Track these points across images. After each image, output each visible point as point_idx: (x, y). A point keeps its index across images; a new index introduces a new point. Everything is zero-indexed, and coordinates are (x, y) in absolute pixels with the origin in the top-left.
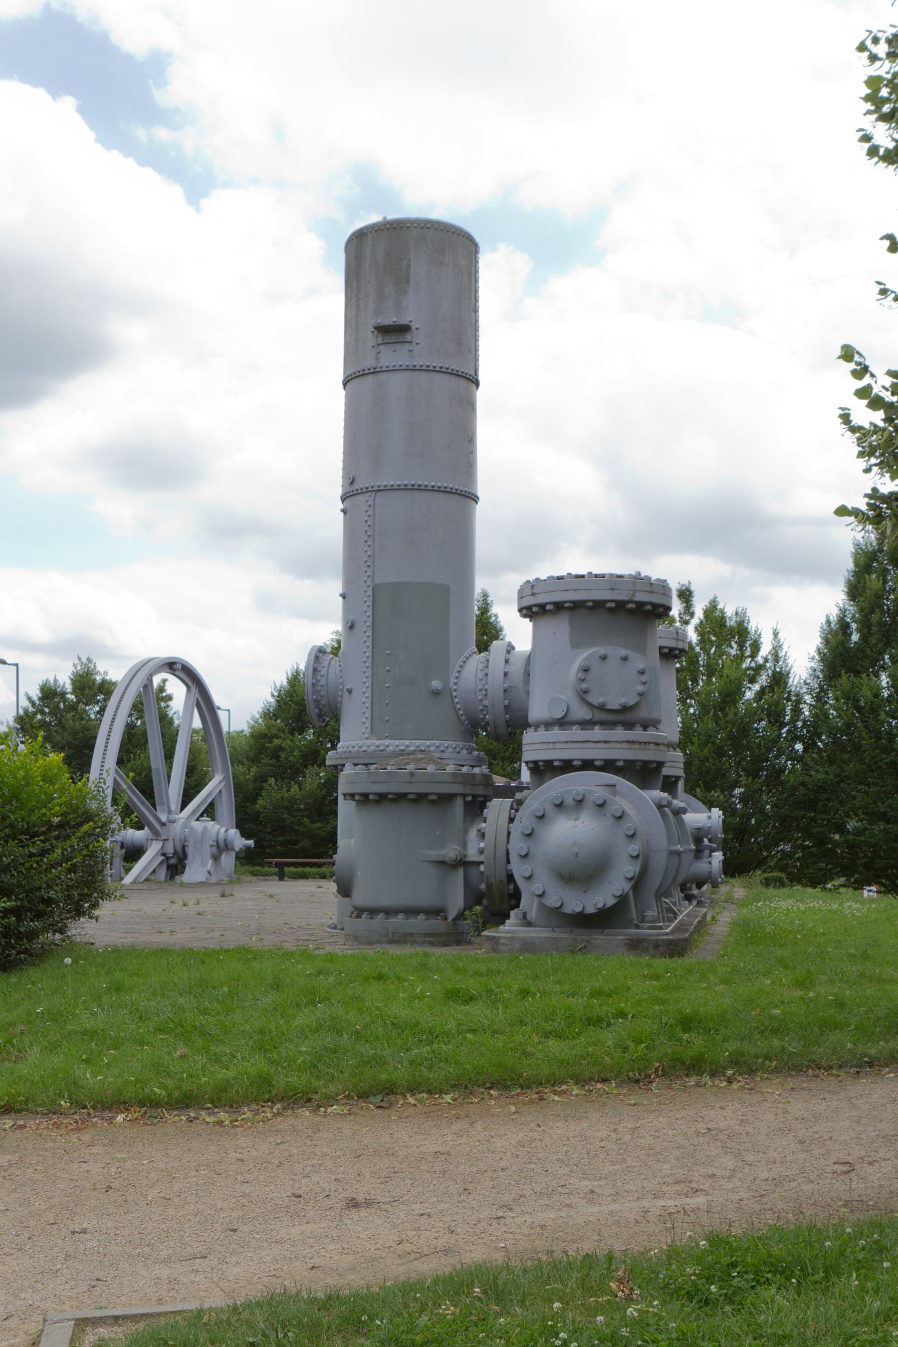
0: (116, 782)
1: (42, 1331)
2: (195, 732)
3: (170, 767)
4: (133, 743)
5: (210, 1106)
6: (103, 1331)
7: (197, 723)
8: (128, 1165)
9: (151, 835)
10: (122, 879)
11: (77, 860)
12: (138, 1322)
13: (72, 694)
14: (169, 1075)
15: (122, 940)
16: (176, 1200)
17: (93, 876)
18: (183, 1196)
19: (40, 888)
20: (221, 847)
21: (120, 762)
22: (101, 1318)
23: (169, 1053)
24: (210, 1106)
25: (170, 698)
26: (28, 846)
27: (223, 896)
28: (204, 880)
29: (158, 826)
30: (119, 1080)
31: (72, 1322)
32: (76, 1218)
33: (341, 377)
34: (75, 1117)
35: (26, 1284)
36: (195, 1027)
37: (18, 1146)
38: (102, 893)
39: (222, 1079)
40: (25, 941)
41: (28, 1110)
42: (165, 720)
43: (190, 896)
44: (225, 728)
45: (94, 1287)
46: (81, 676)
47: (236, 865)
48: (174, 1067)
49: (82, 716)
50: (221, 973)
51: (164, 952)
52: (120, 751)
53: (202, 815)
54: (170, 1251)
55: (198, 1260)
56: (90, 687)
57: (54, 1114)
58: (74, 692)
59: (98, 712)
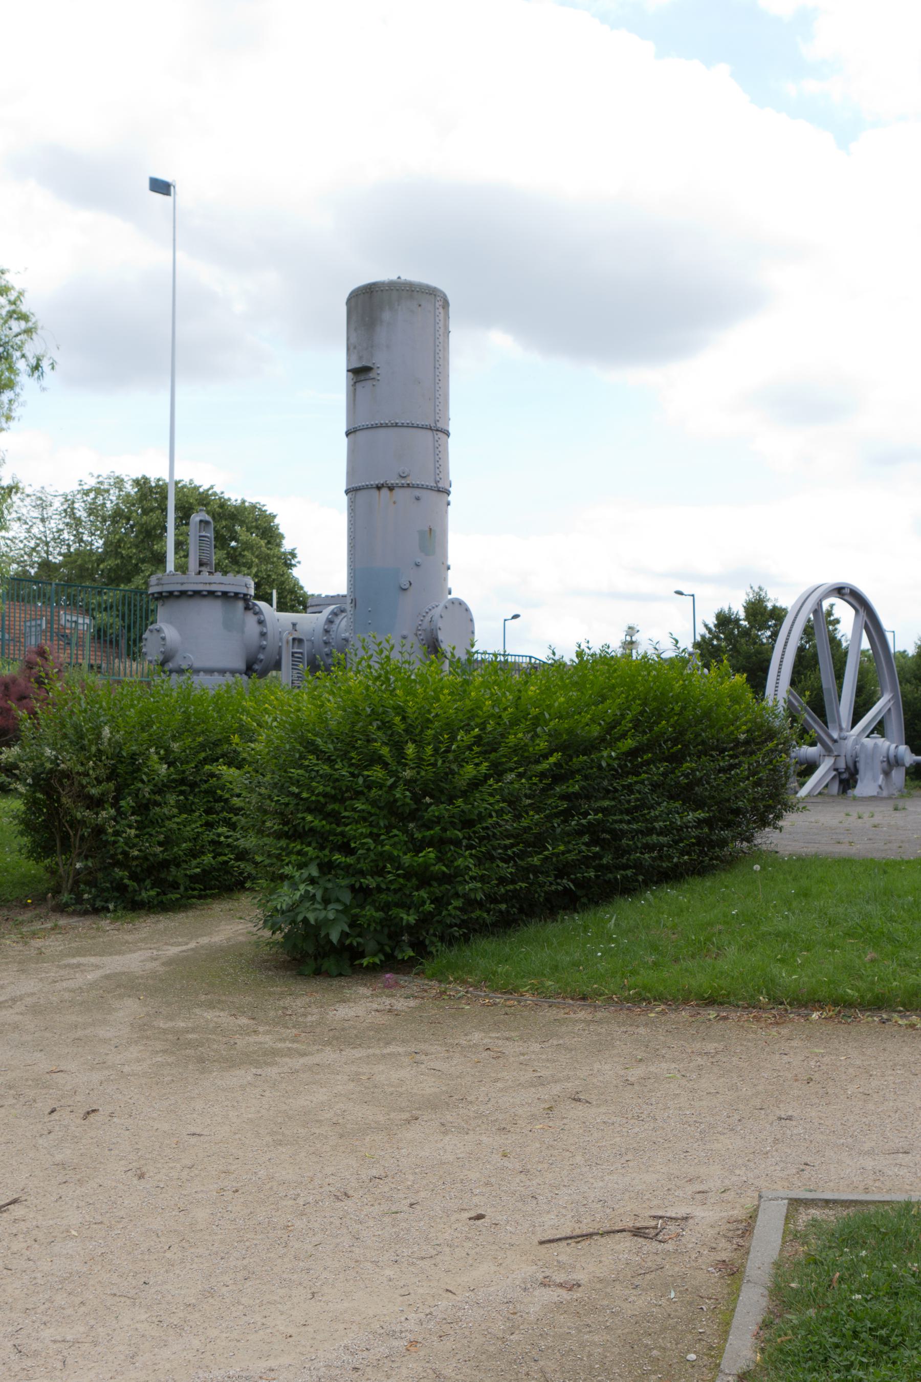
0: (789, 703)
1: (758, 1206)
2: (863, 653)
3: (840, 687)
4: (805, 663)
5: (902, 1009)
6: (814, 1212)
7: (865, 644)
8: (826, 1060)
9: (823, 752)
10: (797, 793)
11: (763, 774)
12: (848, 1208)
13: (745, 620)
14: (861, 977)
15: (805, 849)
16: (875, 1096)
17: (777, 789)
18: (881, 1093)
19: (728, 800)
20: (892, 763)
21: (793, 683)
22: (813, 1200)
23: (859, 957)
24: (902, 1009)
25: (837, 621)
26: (718, 760)
27: (896, 809)
28: (875, 794)
29: (830, 743)
30: (814, 980)
31: (786, 1201)
32: (781, 1106)
33: (344, 429)
34: (773, 1012)
35: (740, 1161)
36: (882, 933)
37: (723, 1036)
38: (785, 805)
39: (913, 984)
40: (717, 849)
41: (729, 1003)
42: (834, 643)
43: (864, 810)
44: (892, 651)
45: (803, 1170)
46: (753, 603)
47: (906, 780)
48: (865, 970)
49: (755, 640)
50: (905, 883)
51: (846, 862)
52: (793, 673)
53: (872, 732)
54: (873, 1144)
55: (901, 1155)
56: (762, 614)
57: (754, 1008)
58: (747, 618)
59: (770, 637)
